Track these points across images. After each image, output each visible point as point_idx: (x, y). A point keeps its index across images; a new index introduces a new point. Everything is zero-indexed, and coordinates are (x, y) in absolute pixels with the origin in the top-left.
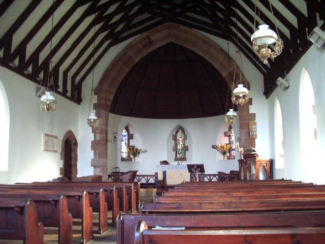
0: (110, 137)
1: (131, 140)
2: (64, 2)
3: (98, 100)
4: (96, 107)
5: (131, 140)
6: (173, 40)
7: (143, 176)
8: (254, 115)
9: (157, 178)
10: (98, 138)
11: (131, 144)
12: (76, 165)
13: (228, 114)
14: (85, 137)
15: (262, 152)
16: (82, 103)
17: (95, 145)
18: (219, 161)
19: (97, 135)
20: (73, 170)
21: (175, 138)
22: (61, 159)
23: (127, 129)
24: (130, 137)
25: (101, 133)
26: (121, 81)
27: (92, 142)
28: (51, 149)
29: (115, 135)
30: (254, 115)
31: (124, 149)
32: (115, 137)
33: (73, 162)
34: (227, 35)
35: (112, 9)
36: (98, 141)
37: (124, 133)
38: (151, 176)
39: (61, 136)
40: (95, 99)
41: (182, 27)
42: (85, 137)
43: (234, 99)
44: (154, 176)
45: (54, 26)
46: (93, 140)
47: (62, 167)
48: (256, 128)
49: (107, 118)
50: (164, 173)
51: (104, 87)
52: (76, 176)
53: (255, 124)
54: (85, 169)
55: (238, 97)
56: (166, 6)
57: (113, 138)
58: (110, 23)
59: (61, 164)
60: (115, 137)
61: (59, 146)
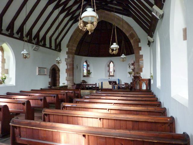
0: (75, 67)
1: (88, 67)
2: (28, 1)
3: (68, 50)
4: (67, 53)
5: (88, 67)
6: (103, 19)
7: (90, 85)
8: (142, 55)
9: (96, 85)
10: (68, 68)
11: (88, 69)
12: (59, 80)
13: (122, 56)
14: (63, 67)
15: (145, 75)
16: (61, 51)
17: (67, 70)
18: (129, 77)
19: (68, 66)
20: (57, 82)
21: (109, 66)
22: (49, 78)
23: (86, 62)
24: (88, 66)
25: (70, 65)
26: (79, 40)
27: (66, 69)
28: (43, 74)
29: (77, 66)
30: (142, 55)
31: (85, 72)
32: (77, 67)
33: (57, 78)
34: (129, 15)
35: (70, 3)
36: (69, 69)
37: (85, 64)
38: (94, 85)
39: (49, 67)
40: (67, 50)
41: (106, 12)
42: (63, 67)
43: (111, 51)
44: (95, 84)
45: (27, 14)
46: (66, 68)
47: (50, 81)
48: (143, 63)
49: (73, 58)
50: (102, 83)
51: (70, 44)
52: (59, 85)
53: (143, 60)
54: (63, 80)
55: (113, 50)
56: (103, 3)
57: (76, 67)
58: (70, 12)
59: (50, 80)
60: (77, 67)
61: (47, 72)
